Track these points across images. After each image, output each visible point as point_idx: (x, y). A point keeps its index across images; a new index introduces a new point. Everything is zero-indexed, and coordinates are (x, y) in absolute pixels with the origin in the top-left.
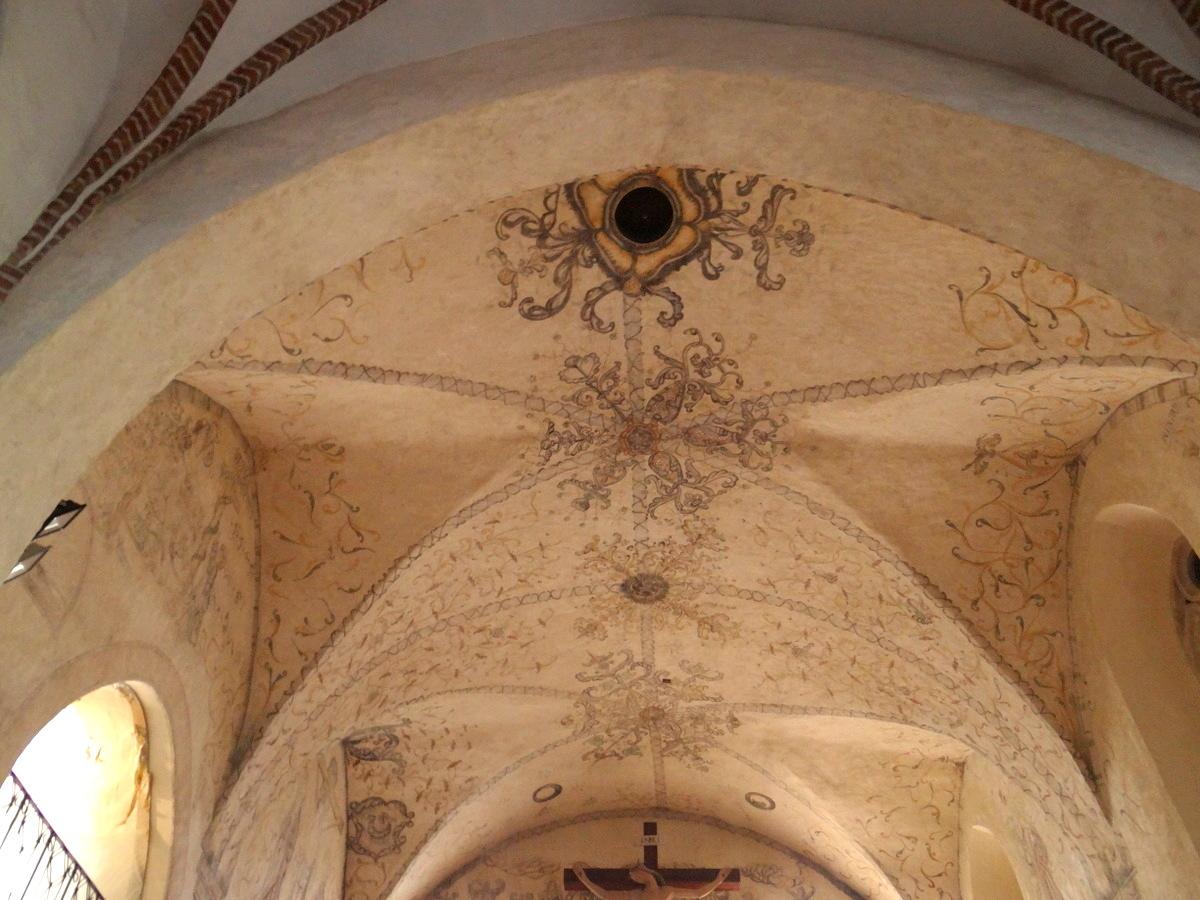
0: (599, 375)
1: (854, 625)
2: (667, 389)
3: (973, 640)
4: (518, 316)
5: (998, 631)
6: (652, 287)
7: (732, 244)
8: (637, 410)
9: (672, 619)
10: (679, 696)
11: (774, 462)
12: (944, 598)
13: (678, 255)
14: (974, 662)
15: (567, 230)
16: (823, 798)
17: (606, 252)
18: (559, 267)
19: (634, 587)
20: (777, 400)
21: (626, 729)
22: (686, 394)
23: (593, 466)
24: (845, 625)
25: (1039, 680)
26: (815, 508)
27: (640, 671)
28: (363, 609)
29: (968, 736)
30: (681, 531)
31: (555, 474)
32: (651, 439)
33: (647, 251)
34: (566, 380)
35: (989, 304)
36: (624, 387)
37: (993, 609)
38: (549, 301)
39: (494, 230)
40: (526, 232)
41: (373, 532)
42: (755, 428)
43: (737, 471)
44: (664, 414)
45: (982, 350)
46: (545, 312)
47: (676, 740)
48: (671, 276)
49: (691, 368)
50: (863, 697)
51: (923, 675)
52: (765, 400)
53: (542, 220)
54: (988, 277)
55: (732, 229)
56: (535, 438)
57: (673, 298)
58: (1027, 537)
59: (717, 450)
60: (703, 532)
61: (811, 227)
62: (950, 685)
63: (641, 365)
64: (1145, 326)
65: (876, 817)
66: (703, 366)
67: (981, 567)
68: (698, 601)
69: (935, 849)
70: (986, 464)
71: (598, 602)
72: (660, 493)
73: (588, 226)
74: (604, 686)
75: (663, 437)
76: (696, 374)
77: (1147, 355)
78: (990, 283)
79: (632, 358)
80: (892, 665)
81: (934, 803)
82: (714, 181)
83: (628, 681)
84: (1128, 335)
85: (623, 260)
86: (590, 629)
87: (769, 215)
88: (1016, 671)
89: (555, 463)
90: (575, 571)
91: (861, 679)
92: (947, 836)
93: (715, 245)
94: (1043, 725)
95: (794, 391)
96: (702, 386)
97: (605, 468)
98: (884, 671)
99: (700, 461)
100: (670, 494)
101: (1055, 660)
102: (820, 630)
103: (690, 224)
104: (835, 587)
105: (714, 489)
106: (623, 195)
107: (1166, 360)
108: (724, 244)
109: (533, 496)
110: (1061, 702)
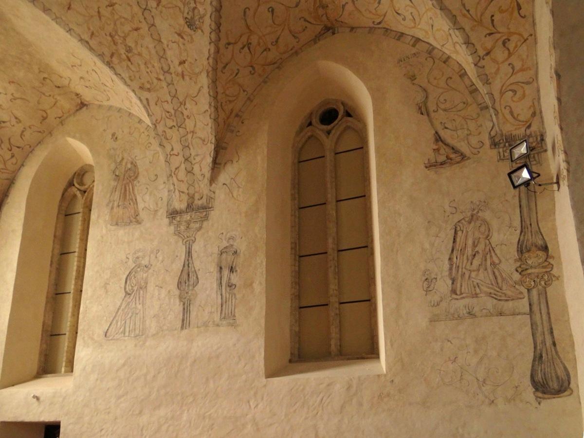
3: (211, 60)
5: (224, 67)
12: (219, 25)
14: (197, 70)
25: (223, 105)
29: (147, 99)
37: (233, 55)
51: (153, 52)
58: (278, 38)
64: (479, 16)
65: (6, 94)
67: (248, 31)
69: (27, 134)
77: (464, 27)
80: (137, 29)
81: (48, 112)
84: (468, 11)
88: (217, 92)
92: (40, 132)
94: (210, 125)
98: (127, 28)
101: (236, 101)
107: (468, 37)
110: (224, 122)
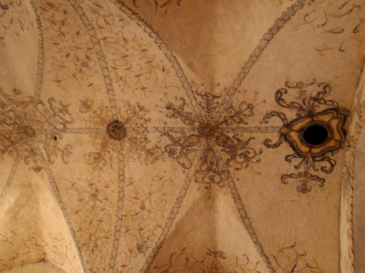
0: (242, 117)
1: (121, 219)
2: (233, 142)
4: (279, 88)
6: (283, 138)
7: (301, 166)
8: (222, 131)
9: (99, 141)
10: (46, 144)
11: (200, 183)
13: (297, 146)
15: (316, 108)
16: (6, 214)
17: (302, 121)
18: (299, 104)
19: (116, 126)
20: (231, 183)
21: (15, 119)
22: (230, 149)
23: (192, 112)
24: (120, 216)
26: (180, 200)
27: (61, 127)
28: (123, 8)
30: (155, 146)
31: (189, 97)
32: (207, 136)
33: (300, 136)
34: (241, 104)
35: (293, 257)
36: (235, 126)
38: (283, 100)
39: (324, 82)
40: (319, 93)
41: (166, 11)
42: (216, 175)
43: (193, 168)
44: (220, 140)
45: (274, 257)
46: (278, 98)
47: (12, 142)
48: (287, 144)
49: (243, 151)
50: (82, 227)
51: (110, 253)
52: (230, 179)
53: (323, 99)
54: (303, 255)
55: (307, 166)
56: (212, 90)
57: (277, 144)
59: (203, 161)
60: (155, 155)
61: (309, 193)
62: (112, 265)
63: (246, 132)
66: (245, 155)
68: (112, 152)
70: (211, 255)
71: (105, 110)
72: (176, 138)
73: (315, 115)
74: (46, 110)
75: (208, 140)
76: (241, 153)
78: (301, 256)
79: (249, 129)
81: (20, 256)
82: (327, 159)
83: (52, 121)
85: (297, 127)
86: (86, 105)
87: (313, 178)
89: (196, 97)
90: (127, 101)
91: (91, 225)
92: (4, 265)
93: (300, 160)
95: (237, 190)
96: (234, 155)
97: (191, 117)
99: (196, 154)
100: (176, 142)
102: (112, 205)
103: (310, 151)
104: (139, 210)
105: (181, 159)
106: (326, 127)
108: (301, 163)
109: (177, 87)
